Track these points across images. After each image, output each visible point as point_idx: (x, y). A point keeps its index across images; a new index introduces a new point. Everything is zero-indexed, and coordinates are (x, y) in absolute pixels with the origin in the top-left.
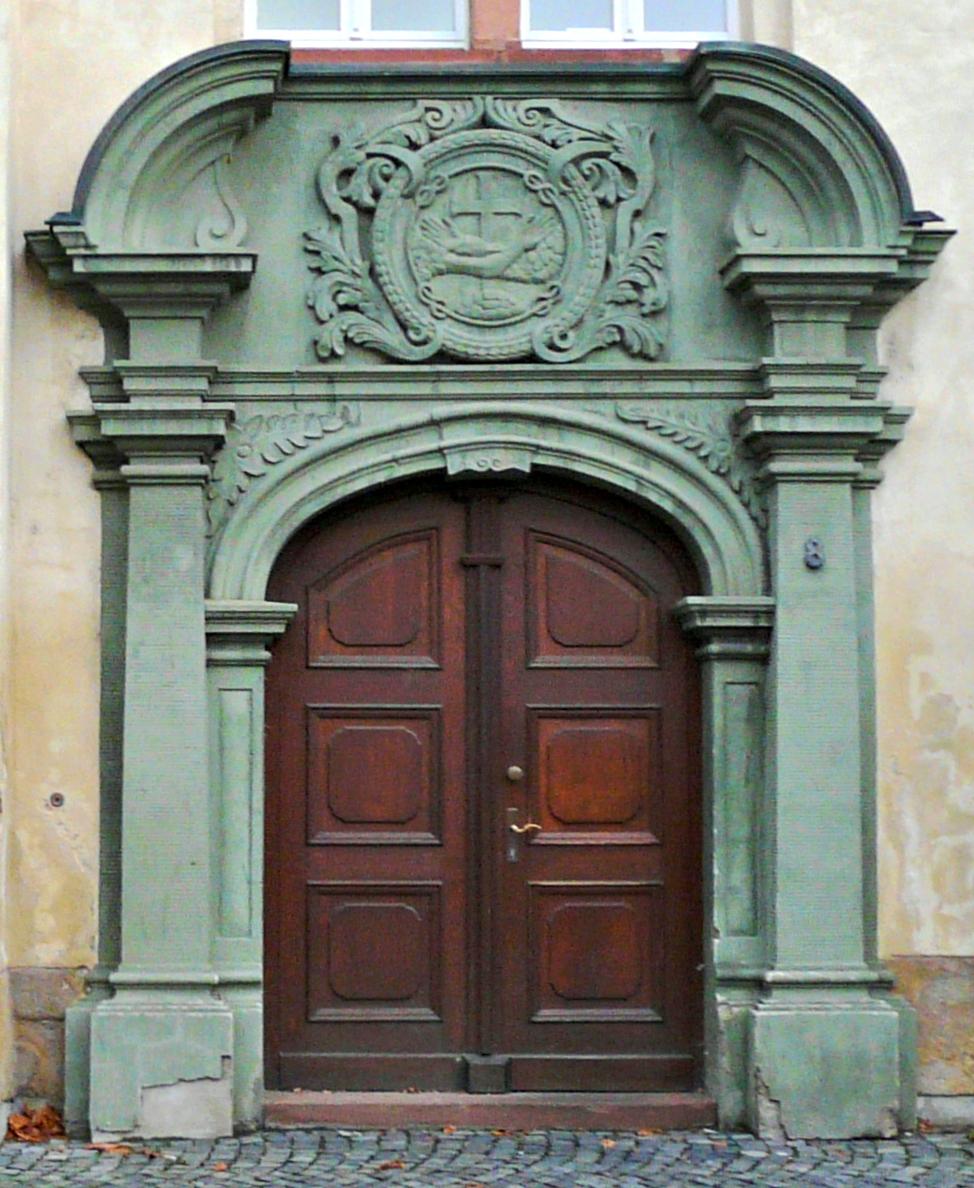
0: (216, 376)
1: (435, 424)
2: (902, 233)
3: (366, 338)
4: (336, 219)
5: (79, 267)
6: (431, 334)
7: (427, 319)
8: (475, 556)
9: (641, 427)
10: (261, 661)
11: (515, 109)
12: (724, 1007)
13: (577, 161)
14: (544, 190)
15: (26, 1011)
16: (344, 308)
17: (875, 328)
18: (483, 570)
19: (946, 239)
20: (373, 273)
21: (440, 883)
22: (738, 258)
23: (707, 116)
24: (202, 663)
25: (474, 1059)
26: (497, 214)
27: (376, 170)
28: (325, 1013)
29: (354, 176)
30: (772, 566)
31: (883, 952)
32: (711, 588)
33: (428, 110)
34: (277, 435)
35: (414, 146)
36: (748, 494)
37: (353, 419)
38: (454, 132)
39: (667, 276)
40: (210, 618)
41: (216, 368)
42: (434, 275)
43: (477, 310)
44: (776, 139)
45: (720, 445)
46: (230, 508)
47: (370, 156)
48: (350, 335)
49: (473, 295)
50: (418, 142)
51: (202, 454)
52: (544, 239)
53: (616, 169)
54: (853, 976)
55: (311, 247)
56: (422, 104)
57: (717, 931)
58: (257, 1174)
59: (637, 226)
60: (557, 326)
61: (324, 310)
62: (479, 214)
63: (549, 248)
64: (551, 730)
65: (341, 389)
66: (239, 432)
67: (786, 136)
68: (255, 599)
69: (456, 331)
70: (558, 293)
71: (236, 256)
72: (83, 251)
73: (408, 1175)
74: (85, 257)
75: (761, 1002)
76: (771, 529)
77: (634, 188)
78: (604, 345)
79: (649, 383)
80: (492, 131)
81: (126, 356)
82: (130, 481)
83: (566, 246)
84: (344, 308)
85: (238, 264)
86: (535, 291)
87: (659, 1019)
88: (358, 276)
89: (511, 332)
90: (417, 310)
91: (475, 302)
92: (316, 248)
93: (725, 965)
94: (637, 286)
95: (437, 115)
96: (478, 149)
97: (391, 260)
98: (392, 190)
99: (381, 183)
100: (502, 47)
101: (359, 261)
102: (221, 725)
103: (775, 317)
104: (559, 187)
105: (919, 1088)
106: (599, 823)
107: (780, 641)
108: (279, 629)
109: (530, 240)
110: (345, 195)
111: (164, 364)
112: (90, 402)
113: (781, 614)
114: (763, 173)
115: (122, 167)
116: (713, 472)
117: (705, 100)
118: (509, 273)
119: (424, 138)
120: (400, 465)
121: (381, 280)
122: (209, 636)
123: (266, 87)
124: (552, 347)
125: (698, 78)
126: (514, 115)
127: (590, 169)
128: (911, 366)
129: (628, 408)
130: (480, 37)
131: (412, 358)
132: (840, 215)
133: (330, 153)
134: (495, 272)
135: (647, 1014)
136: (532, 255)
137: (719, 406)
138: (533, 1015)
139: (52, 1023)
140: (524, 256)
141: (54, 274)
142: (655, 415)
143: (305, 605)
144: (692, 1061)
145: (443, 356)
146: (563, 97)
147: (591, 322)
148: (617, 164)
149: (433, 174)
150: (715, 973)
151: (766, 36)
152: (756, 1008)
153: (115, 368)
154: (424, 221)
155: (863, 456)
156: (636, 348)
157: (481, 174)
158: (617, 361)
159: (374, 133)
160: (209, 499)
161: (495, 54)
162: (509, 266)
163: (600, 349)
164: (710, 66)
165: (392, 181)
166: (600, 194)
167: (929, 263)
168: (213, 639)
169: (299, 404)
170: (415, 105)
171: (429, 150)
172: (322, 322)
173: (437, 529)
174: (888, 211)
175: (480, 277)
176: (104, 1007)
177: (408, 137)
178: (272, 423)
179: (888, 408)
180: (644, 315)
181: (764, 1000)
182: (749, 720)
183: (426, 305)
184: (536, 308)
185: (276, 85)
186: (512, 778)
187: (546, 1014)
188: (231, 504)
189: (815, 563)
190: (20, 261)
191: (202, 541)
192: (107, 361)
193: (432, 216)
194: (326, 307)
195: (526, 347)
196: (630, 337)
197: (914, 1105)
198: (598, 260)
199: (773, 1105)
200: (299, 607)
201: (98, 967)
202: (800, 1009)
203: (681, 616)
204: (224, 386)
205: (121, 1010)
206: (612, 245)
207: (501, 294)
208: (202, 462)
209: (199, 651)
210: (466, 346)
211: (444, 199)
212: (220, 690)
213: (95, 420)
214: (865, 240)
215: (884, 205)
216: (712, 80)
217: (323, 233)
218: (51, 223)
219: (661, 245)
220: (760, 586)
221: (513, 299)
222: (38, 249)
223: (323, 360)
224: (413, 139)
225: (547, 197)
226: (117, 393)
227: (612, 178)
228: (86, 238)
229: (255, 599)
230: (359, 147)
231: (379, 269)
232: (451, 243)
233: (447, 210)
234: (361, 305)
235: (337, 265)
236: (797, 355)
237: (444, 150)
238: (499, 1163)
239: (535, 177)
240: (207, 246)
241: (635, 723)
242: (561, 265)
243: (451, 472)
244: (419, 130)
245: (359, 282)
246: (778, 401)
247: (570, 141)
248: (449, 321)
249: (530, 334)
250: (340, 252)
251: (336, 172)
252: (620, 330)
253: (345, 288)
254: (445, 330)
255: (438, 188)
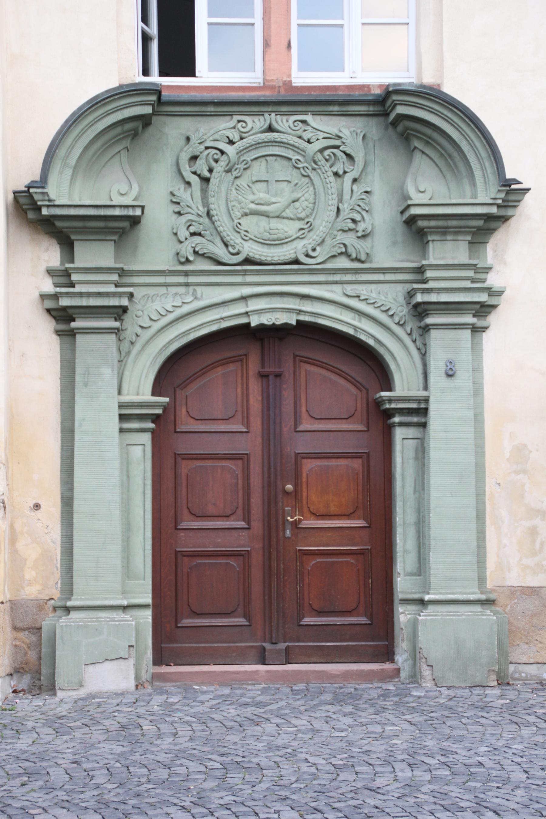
0: (122, 273)
1: (244, 298)
2: (499, 191)
3: (205, 251)
4: (189, 184)
5: (45, 212)
6: (241, 249)
7: (239, 240)
8: (267, 370)
9: (357, 299)
10: (150, 429)
11: (287, 121)
12: (403, 615)
13: (321, 151)
14: (303, 168)
15: (19, 625)
16: (193, 234)
17: (487, 243)
18: (271, 378)
19: (526, 193)
20: (209, 214)
21: (249, 549)
22: (409, 206)
23: (394, 124)
24: (117, 430)
25: (267, 646)
26: (276, 181)
27: (210, 156)
28: (186, 622)
29: (198, 159)
30: (428, 375)
31: (489, 585)
32: (395, 387)
33: (239, 121)
34: (157, 305)
35: (231, 142)
36: (415, 335)
37: (199, 296)
38: (253, 134)
39: (371, 214)
40: (121, 406)
41: (122, 269)
42: (242, 216)
43: (266, 235)
44: (430, 138)
45: (400, 309)
46: (131, 346)
47: (207, 148)
48: (197, 249)
49: (264, 227)
50: (234, 140)
51: (116, 316)
52: (303, 195)
53: (344, 156)
54: (472, 597)
55: (174, 200)
56: (236, 118)
57: (399, 574)
58: (147, 708)
59: (355, 187)
60: (310, 244)
61: (182, 235)
62: (267, 181)
63: (306, 200)
64: (308, 465)
65: (192, 279)
66: (136, 303)
67: (436, 136)
68: (147, 396)
69: (256, 248)
70: (311, 225)
71: (133, 206)
72: (47, 203)
73: (228, 707)
74: (48, 206)
75: (422, 612)
76: (427, 355)
77: (353, 166)
78: (337, 254)
79: (360, 275)
80: (275, 134)
81: (73, 262)
82: (75, 331)
83: (315, 199)
84: (193, 234)
85: (134, 211)
86: (298, 224)
87: (369, 622)
88: (201, 216)
89: (285, 248)
90: (233, 236)
91: (265, 231)
92: (178, 201)
93: (402, 592)
94: (354, 221)
95: (244, 125)
96: (267, 144)
97: (219, 207)
98: (219, 168)
99: (213, 164)
100: (281, 84)
101: (201, 208)
102: (128, 464)
103: (430, 238)
104: (311, 166)
105: (510, 659)
106: (335, 515)
107: (431, 415)
108: (159, 411)
109: (296, 195)
110: (193, 170)
111: (94, 266)
112: (52, 286)
113: (432, 401)
114: (424, 157)
115: (67, 157)
116: (396, 324)
117: (392, 116)
118: (284, 214)
119: (236, 138)
120: (225, 321)
121: (213, 218)
122: (120, 415)
123: (148, 110)
124: (307, 255)
125: (389, 103)
126: (286, 124)
127: (329, 155)
128: (505, 264)
129: (350, 289)
130: (268, 78)
131: (231, 262)
132: (466, 181)
133: (185, 146)
134: (277, 214)
135: (363, 620)
136: (297, 204)
137: (400, 287)
138: (301, 621)
139: (35, 631)
140: (292, 205)
141: (31, 215)
142: (365, 292)
143: (174, 400)
144: (387, 645)
145: (248, 261)
146: (314, 114)
147: (328, 241)
148: (344, 152)
149: (242, 159)
150: (398, 596)
151: (428, 79)
152: (420, 615)
153: (66, 268)
154: (237, 185)
155: (477, 314)
156: (354, 256)
157: (268, 158)
158: (343, 263)
159: (209, 135)
160: (120, 340)
161: (277, 89)
162: (284, 211)
163: (334, 256)
164: (395, 97)
165: (219, 162)
166: (335, 169)
167: (515, 207)
168: (123, 418)
169: (169, 288)
170: (232, 118)
171: (240, 145)
172: (181, 242)
173: (246, 355)
174: (492, 179)
175: (268, 217)
176: (64, 620)
177: (228, 137)
178: (154, 298)
179: (491, 288)
180: (358, 237)
181: (424, 611)
182: (416, 458)
183: (239, 233)
184: (299, 234)
185: (153, 109)
186: (287, 491)
187: (308, 620)
188: (132, 343)
189: (451, 373)
190: (11, 209)
191: (116, 363)
192: (62, 263)
193: (241, 182)
194: (183, 233)
195: (293, 256)
196: (351, 250)
197: (507, 669)
198: (333, 207)
199: (429, 668)
200: (170, 400)
201: (60, 599)
202: (442, 615)
203: (378, 403)
204: (128, 278)
205: (73, 622)
206: (340, 200)
207: (280, 226)
208: (116, 320)
209: (115, 423)
210: (261, 255)
211: (248, 172)
212: (128, 445)
213: (56, 297)
214: (479, 195)
215: (490, 176)
216: (396, 105)
217: (183, 194)
218: (29, 187)
219: (368, 197)
220: (421, 386)
221: (286, 229)
222: (22, 201)
223: (182, 263)
224: (231, 138)
225: (305, 171)
226: (68, 282)
227: (341, 160)
228: (48, 195)
229: (147, 396)
230: (200, 143)
231: (212, 213)
232: (252, 197)
233: (250, 179)
234: (202, 233)
235: (189, 210)
236: (442, 258)
237: (248, 145)
238: (279, 700)
239: (299, 160)
240: (118, 200)
241: (356, 460)
242: (313, 210)
243: (253, 325)
244: (234, 133)
245: (201, 220)
246: (431, 285)
247: (318, 140)
248: (251, 241)
249: (296, 248)
250: (190, 203)
251: (189, 157)
252: (345, 245)
253: (193, 223)
254: (249, 247)
255: (245, 166)
